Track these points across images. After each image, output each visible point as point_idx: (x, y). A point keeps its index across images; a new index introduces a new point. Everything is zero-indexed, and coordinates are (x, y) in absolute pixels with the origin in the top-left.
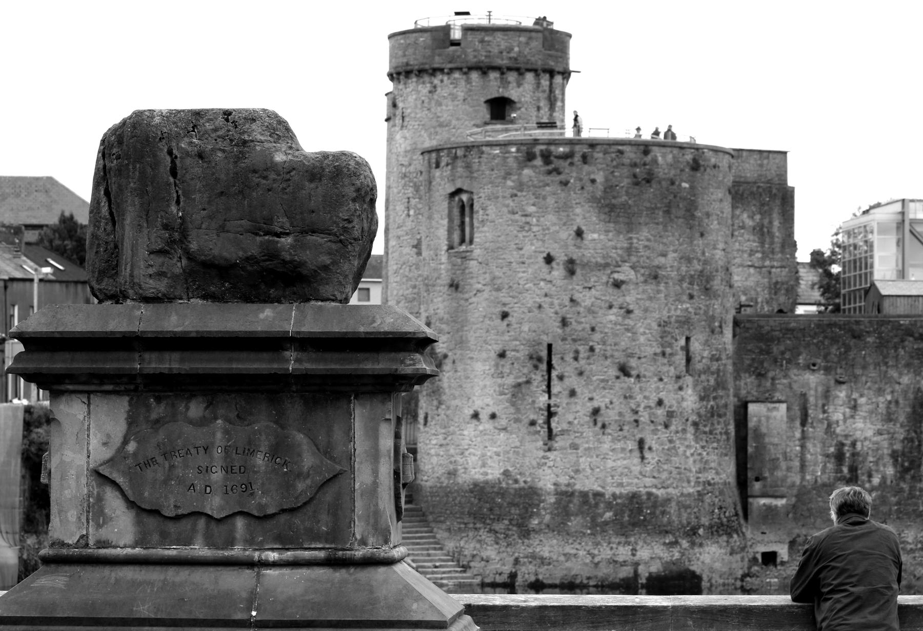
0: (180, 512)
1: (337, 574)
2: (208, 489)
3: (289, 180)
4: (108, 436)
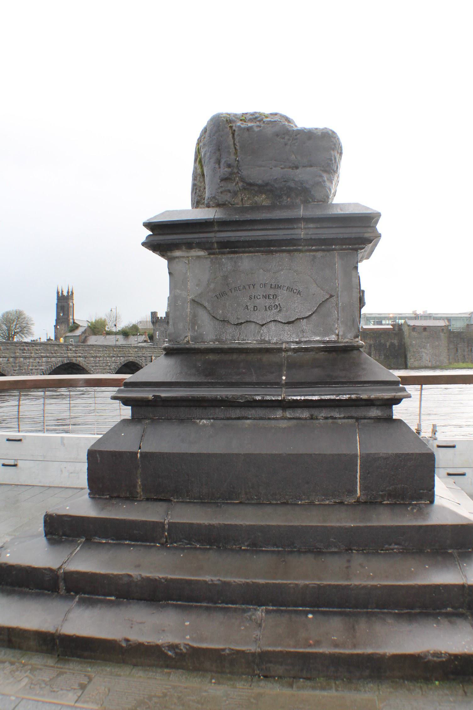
2: (256, 308)
4: (199, 280)
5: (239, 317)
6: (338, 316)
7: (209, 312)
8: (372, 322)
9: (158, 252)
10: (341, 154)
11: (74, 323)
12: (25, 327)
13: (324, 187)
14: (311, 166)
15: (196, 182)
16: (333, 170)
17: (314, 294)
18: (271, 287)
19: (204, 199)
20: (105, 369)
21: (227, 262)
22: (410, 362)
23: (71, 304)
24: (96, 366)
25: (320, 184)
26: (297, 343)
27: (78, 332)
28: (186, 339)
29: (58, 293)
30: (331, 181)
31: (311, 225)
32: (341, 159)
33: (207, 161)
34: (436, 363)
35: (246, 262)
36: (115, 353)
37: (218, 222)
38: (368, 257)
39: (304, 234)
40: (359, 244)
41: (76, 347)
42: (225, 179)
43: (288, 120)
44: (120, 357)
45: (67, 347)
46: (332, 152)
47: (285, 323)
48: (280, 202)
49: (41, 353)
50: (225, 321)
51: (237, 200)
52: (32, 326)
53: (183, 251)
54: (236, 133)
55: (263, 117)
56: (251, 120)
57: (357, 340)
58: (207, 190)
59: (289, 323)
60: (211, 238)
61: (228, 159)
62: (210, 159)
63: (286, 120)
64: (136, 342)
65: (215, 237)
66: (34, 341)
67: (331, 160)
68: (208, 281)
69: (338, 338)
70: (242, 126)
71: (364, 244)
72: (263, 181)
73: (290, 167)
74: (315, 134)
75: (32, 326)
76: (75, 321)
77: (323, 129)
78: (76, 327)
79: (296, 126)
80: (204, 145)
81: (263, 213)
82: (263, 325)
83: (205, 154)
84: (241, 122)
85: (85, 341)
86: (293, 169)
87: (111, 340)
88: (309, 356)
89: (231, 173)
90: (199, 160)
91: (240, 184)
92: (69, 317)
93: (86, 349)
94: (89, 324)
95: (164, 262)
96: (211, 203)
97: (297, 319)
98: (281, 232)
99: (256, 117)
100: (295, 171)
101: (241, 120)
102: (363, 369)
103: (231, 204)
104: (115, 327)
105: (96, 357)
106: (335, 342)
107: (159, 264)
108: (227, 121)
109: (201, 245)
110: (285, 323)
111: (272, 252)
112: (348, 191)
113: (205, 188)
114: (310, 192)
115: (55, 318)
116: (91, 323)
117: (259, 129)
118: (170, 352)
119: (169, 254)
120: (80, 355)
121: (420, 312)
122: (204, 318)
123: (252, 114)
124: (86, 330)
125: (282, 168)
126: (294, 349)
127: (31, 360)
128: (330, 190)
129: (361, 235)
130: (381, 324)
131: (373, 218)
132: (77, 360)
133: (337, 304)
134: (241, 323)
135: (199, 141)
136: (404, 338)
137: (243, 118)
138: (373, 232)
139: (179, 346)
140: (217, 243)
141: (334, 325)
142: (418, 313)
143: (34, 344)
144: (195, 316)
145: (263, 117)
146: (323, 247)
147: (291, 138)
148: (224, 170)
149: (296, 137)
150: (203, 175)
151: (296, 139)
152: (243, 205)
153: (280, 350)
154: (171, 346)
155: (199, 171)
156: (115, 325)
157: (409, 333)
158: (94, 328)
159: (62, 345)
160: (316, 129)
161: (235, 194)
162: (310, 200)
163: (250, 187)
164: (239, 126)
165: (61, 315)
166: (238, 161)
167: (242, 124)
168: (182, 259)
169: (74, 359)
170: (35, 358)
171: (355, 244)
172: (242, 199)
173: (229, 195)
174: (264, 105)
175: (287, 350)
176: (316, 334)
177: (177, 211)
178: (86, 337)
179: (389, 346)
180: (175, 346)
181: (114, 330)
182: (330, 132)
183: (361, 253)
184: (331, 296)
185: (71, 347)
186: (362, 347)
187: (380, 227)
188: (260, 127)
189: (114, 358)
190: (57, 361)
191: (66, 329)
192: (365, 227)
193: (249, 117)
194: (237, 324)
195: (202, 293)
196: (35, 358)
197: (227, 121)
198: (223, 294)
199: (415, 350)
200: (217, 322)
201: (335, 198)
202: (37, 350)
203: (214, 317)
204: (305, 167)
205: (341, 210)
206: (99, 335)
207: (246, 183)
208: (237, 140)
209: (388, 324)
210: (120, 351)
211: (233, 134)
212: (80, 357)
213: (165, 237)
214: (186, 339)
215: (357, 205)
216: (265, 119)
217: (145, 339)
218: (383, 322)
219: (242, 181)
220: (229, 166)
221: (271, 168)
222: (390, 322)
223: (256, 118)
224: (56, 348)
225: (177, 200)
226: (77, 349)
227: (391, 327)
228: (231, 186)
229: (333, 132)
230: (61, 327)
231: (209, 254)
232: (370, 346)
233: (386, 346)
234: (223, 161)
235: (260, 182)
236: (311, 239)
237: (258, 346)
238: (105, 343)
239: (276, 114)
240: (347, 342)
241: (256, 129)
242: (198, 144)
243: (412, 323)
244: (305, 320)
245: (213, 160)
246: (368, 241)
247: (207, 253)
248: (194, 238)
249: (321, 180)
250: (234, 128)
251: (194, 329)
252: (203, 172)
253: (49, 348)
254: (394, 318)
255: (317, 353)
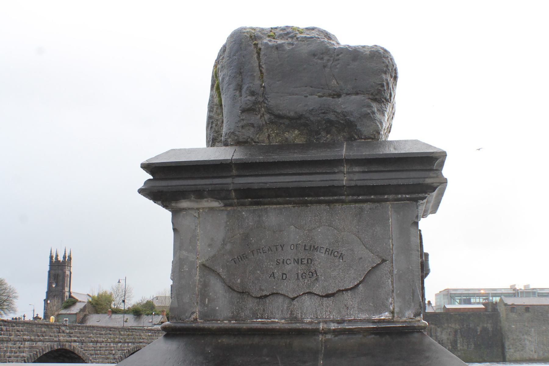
0: (264, 293)
1: (384, 339)
2: (284, 276)
3: (338, 60)
4: (212, 239)
5: (263, 288)
6: (393, 287)
7: (223, 281)
8: (458, 301)
9: (159, 202)
10: (395, 78)
11: (70, 296)
12: (5, 301)
13: (373, 120)
14: (357, 94)
15: (212, 114)
16: (385, 99)
17: (361, 258)
18: (305, 249)
19: (221, 136)
20: (108, 358)
21: (248, 215)
22: (510, 352)
23: (68, 273)
24: (96, 354)
25: (368, 117)
26: (339, 322)
27: (75, 310)
28: (193, 316)
29: (51, 257)
30: (383, 113)
31: (356, 169)
32: (396, 85)
33: (225, 86)
34: (543, 354)
35: (273, 216)
36: (121, 337)
37: (236, 164)
38: (434, 210)
39: (346, 180)
40: (419, 193)
41: (71, 328)
42: (247, 110)
43: (328, 36)
44: (128, 343)
45: (60, 328)
46: (384, 76)
47: (322, 296)
48: (317, 139)
49: (24, 335)
50: (244, 293)
51: (263, 137)
52: (15, 300)
53: (191, 201)
54: (262, 53)
55: (297, 32)
56: (281, 36)
57: (418, 318)
58: (224, 125)
59: (328, 296)
60: (227, 184)
61: (251, 85)
62: (229, 85)
63: (325, 36)
64: (151, 324)
65: (233, 183)
66: (16, 319)
67: (383, 86)
68: (224, 241)
69: (393, 316)
70: (270, 43)
71: (426, 193)
72: (296, 113)
73: (330, 95)
74: (362, 53)
75: (15, 300)
76: (72, 295)
77: (372, 47)
78: (73, 302)
79: (338, 44)
80: (222, 67)
81: (295, 153)
82: (293, 299)
83: (223, 79)
84: (268, 39)
85: (83, 321)
86: (333, 98)
87: (117, 321)
88: (353, 340)
89: (256, 103)
90: (216, 87)
91: (267, 117)
92: (64, 288)
93: (85, 331)
94: (90, 300)
95: (167, 214)
96: (229, 140)
97: (339, 291)
98: (318, 178)
99: (287, 33)
100: (337, 100)
101: (269, 36)
102: (427, 358)
103: (255, 142)
104: (123, 304)
105: (97, 342)
106: (388, 321)
107: (161, 216)
108: (251, 37)
109: (217, 194)
110: (322, 296)
111: (306, 203)
112: (406, 126)
113: (223, 122)
114: (356, 126)
115: (46, 290)
116: (93, 298)
117: (291, 47)
118: (171, 333)
119: (173, 204)
120: (76, 338)
121: (520, 286)
122: (217, 288)
123: (283, 29)
124: (85, 307)
125: (320, 96)
126: (334, 331)
127: (10, 345)
128: (381, 123)
129: (421, 181)
130: (470, 303)
131: (436, 159)
132: (71, 346)
133: (391, 272)
134: (266, 296)
135: (217, 62)
136: (500, 322)
137: (272, 34)
138: (437, 177)
139: (182, 325)
140: (235, 190)
141: (387, 299)
142: (518, 287)
143: (16, 322)
144: (205, 285)
145: (297, 32)
146: (372, 197)
147: (332, 59)
148: (246, 99)
149: (338, 57)
150: (221, 105)
151: (338, 60)
152: (270, 142)
153: (315, 332)
154: (173, 325)
155: (216, 100)
156: (124, 301)
157: (507, 315)
158: (97, 304)
159: (52, 325)
160: (364, 47)
161: (260, 129)
162: (356, 137)
163: (278, 119)
164: (266, 44)
165: (54, 286)
166: (264, 87)
167: (270, 41)
168: (190, 212)
169: (67, 344)
170: (15, 342)
171: (414, 193)
172: (269, 136)
173: (252, 130)
174: (300, 19)
175: (326, 332)
176: (361, 310)
177: (185, 149)
178: (85, 316)
179: (481, 331)
180: (178, 325)
181: (122, 307)
182: (382, 51)
183: (422, 205)
184: (384, 261)
185: (63, 328)
186: (425, 328)
187: (446, 172)
188: (293, 44)
189: (120, 344)
190: (44, 346)
191: (60, 304)
192: (426, 170)
193: (278, 32)
194: (260, 298)
195: (214, 256)
196: (15, 342)
197: (251, 37)
198: (243, 257)
199: (515, 337)
200: (235, 294)
201: (390, 135)
202: (18, 331)
203: (229, 287)
204: (349, 94)
205: (395, 149)
206: (102, 313)
207: (273, 115)
208: (263, 61)
209: (478, 303)
210: (128, 335)
211: (259, 54)
212: (75, 341)
213: (168, 182)
214: (193, 316)
215: (416, 142)
216: (299, 35)
217: (162, 320)
218: (472, 300)
219: (269, 113)
220: (253, 93)
221: (306, 97)
222: (481, 301)
223: (288, 33)
224: (43, 329)
225: (188, 137)
226: (71, 331)
227: (482, 306)
228: (255, 119)
229: (386, 51)
230: (56, 302)
231: (226, 205)
232: (456, 332)
233: (477, 332)
234: (245, 87)
235: (292, 114)
236: (356, 186)
237: (287, 326)
238: (110, 325)
239: (313, 29)
240: (405, 322)
241: (288, 48)
242: (215, 66)
243: (510, 301)
244: (349, 292)
245: (232, 87)
246: (431, 188)
247: (222, 205)
248: (206, 185)
249: (369, 111)
250: (259, 46)
251: (204, 304)
252: (220, 101)
253: (35, 329)
254: (486, 295)
255: (364, 336)
